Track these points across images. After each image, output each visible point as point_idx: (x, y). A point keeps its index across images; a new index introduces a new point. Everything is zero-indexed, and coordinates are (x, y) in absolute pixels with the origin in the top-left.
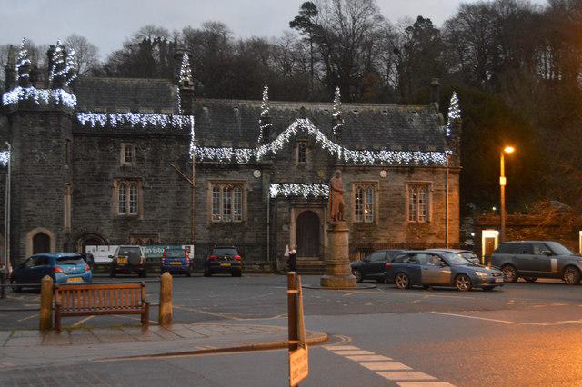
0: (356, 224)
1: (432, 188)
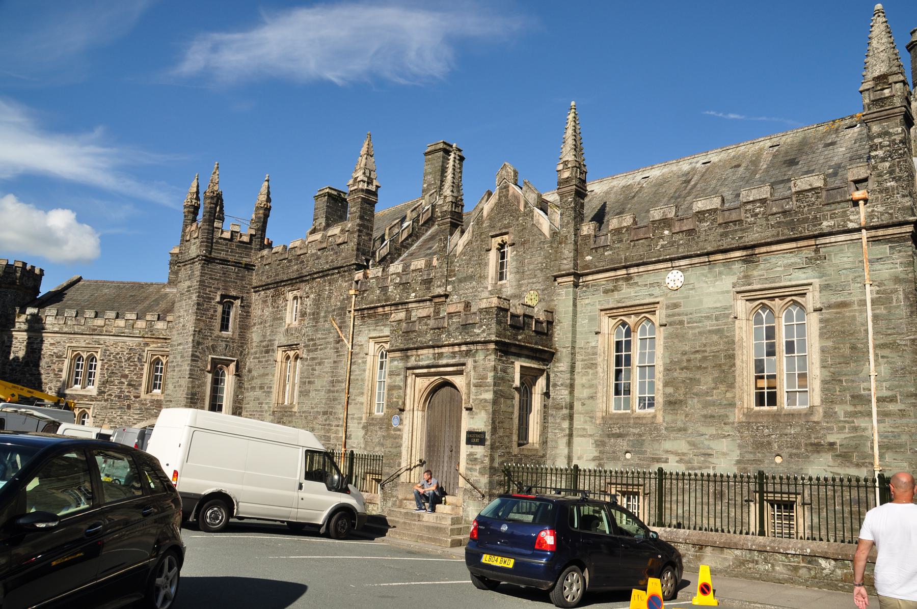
0: (609, 420)
1: (812, 299)
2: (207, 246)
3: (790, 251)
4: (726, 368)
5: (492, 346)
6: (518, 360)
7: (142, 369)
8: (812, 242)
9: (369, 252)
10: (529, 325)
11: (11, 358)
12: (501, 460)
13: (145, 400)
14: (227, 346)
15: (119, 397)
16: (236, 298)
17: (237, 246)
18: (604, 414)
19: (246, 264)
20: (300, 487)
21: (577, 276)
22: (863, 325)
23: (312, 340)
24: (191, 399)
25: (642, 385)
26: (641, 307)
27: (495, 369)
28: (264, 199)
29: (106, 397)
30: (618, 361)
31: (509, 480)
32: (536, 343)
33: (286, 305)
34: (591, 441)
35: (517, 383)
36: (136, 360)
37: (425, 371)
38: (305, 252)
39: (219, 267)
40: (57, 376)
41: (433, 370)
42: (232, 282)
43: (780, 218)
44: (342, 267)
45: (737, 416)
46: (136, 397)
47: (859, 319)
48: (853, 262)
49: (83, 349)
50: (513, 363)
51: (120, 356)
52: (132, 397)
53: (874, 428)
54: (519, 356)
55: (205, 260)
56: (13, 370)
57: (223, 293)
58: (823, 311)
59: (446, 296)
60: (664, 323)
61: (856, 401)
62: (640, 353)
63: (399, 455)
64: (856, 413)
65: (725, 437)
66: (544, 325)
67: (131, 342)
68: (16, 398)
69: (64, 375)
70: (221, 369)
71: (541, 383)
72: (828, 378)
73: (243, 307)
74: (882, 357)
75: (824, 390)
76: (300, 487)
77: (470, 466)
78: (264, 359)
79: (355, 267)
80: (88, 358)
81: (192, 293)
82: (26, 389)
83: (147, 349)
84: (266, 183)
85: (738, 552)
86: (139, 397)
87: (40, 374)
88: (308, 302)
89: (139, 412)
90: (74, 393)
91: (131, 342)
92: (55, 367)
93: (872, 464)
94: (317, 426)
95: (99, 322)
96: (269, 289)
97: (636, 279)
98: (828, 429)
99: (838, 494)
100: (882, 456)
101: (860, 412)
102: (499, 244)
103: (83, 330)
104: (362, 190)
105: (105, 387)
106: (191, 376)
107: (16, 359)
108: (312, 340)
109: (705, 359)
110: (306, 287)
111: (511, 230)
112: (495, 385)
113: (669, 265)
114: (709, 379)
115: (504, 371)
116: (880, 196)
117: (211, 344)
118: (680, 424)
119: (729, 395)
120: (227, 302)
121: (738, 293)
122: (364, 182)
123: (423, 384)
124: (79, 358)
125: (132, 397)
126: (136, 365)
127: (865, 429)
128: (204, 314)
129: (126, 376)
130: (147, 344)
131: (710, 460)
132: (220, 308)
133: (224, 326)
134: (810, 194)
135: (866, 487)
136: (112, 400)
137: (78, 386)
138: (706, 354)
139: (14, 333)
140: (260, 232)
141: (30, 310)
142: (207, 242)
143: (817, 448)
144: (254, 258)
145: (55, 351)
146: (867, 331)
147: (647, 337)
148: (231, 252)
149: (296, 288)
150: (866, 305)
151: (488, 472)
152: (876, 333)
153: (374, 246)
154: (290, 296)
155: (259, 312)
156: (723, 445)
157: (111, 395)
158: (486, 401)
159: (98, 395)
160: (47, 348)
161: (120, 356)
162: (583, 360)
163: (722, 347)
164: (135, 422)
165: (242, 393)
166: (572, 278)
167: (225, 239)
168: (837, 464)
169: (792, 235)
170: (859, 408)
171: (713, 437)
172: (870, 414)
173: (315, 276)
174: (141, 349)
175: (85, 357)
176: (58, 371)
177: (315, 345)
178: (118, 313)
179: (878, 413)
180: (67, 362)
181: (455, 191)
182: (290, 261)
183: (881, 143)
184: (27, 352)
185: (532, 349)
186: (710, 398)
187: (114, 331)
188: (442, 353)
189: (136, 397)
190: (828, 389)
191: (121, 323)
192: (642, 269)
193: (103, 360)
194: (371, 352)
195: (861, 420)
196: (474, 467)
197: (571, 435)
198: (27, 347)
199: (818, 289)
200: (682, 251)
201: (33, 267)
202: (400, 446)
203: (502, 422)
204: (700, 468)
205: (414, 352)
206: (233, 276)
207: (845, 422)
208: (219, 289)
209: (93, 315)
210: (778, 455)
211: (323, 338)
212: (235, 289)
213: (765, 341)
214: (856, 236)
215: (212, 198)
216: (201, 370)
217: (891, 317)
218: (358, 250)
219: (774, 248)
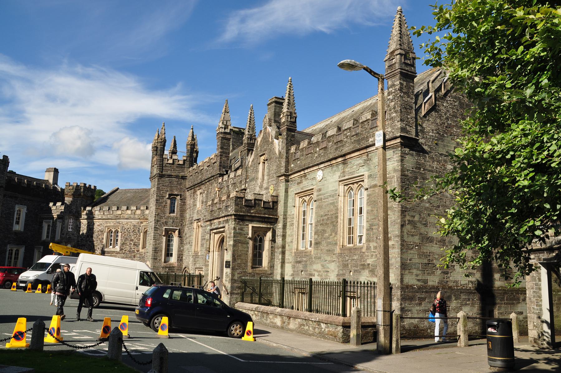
2: (160, 169)
5: (233, 217)
6: (251, 223)
7: (140, 236)
8: (365, 151)
9: (227, 166)
10: (259, 205)
11: (81, 233)
12: (239, 275)
13: (142, 252)
14: (173, 221)
15: (130, 251)
16: (177, 195)
17: (177, 167)
18: (296, 251)
19: (182, 176)
20: (137, 288)
21: (287, 176)
24: (155, 250)
26: (308, 192)
27: (234, 228)
28: (191, 139)
31: (245, 286)
32: (265, 214)
35: (250, 235)
39: (167, 179)
40: (101, 242)
42: (175, 187)
43: (355, 138)
44: (214, 176)
46: (138, 251)
49: (112, 227)
50: (248, 225)
54: (252, 221)
55: (159, 176)
56: (82, 240)
58: (369, 190)
65: (333, 262)
66: (271, 204)
67: (135, 222)
68: (69, 253)
69: (104, 241)
70: (171, 234)
71: (269, 235)
73: (182, 199)
76: (137, 288)
79: (218, 175)
80: (115, 231)
82: (74, 249)
83: (142, 225)
84: (191, 130)
85: (299, 320)
86: (139, 251)
87: (93, 241)
88: (204, 195)
90: (109, 250)
91: (135, 222)
92: (100, 237)
95: (119, 212)
96: (192, 189)
97: (308, 176)
98: (368, 256)
99: (369, 292)
103: (112, 217)
104: (221, 133)
105: (123, 247)
106: (154, 238)
107: (83, 234)
110: (203, 187)
111: (266, 152)
112: (234, 237)
115: (241, 229)
116: (389, 122)
117: (164, 221)
120: (172, 198)
122: (222, 128)
124: (111, 231)
126: (137, 234)
129: (132, 240)
130: (142, 223)
132: (169, 201)
133: (172, 211)
134: (366, 123)
135: (371, 287)
136: (126, 253)
137: (111, 247)
138: (329, 216)
139: (81, 221)
140: (189, 158)
141: (88, 208)
142: (160, 166)
143: (364, 267)
144: (189, 172)
148: (173, 170)
153: (230, 163)
155: (189, 202)
157: (126, 250)
160: (96, 228)
165: (183, 246)
167: (170, 164)
169: (358, 147)
173: (206, 181)
175: (114, 231)
178: (147, 207)
180: (105, 234)
181: (250, 131)
182: (198, 174)
184: (87, 230)
185: (261, 217)
186: (329, 240)
187: (126, 217)
188: (220, 222)
189: (138, 251)
191: (129, 212)
192: (309, 170)
198: (87, 227)
199: (367, 178)
200: (322, 160)
201: (90, 186)
203: (240, 256)
204: (325, 279)
206: (175, 183)
208: (168, 191)
209: (116, 209)
212: (176, 190)
215: (161, 142)
216: (160, 235)
218: (220, 166)
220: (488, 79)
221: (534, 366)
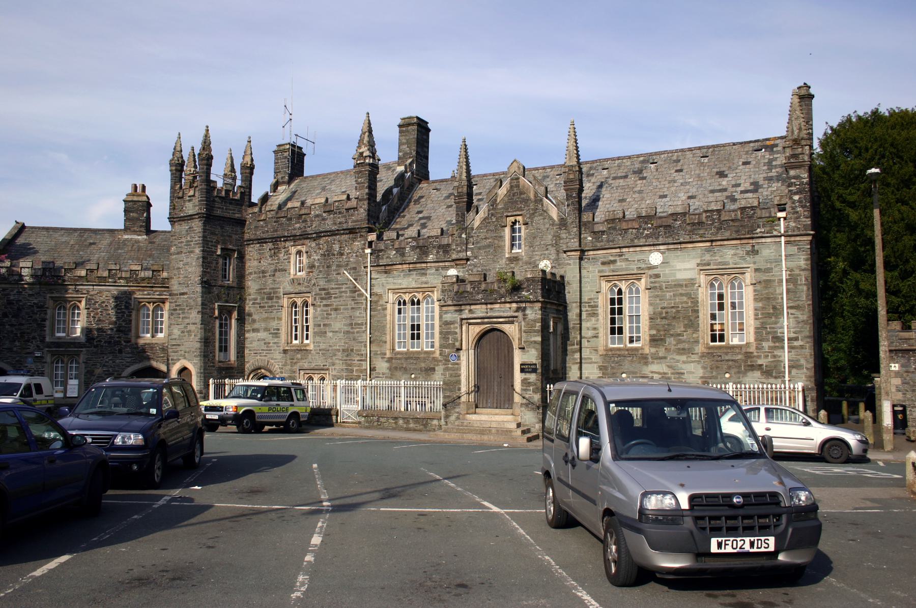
3: (736, 246)
4: (692, 318)
22: (780, 295)
23: (324, 289)
25: (631, 328)
29: (95, 343)
30: (613, 311)
33: (289, 258)
34: (596, 366)
36: (123, 307)
37: (479, 321)
38: (309, 212)
41: (486, 320)
45: (700, 349)
47: (778, 291)
48: (775, 256)
51: (106, 304)
52: (123, 342)
53: (786, 356)
57: (223, 247)
59: (468, 260)
60: (649, 287)
61: (775, 340)
62: (629, 307)
63: (459, 382)
64: (775, 347)
72: (759, 326)
74: (791, 314)
75: (756, 333)
77: (525, 388)
78: (266, 305)
81: (194, 248)
86: (130, 341)
89: (131, 356)
93: (784, 377)
94: (337, 361)
100: (790, 372)
101: (778, 347)
102: (512, 222)
108: (324, 289)
109: (678, 312)
113: (652, 248)
114: (682, 325)
118: (661, 354)
119: (694, 335)
121: (701, 270)
123: (476, 330)
125: (123, 342)
126: (124, 313)
127: (780, 356)
128: (209, 267)
131: (682, 376)
136: (102, 346)
145: (35, 301)
146: (782, 298)
147: (634, 295)
148: (226, 209)
149: (300, 244)
150: (782, 282)
151: (540, 391)
152: (787, 300)
154: (293, 250)
156: (691, 367)
157: (100, 341)
158: (535, 342)
159: (86, 342)
161: (106, 304)
162: (587, 311)
163: (690, 304)
164: (128, 364)
165: (244, 335)
166: (578, 253)
168: (763, 377)
170: (777, 344)
171: (684, 362)
172: (783, 348)
174: (127, 297)
176: (41, 321)
177: (328, 293)
179: (789, 347)
183: (795, 182)
190: (758, 332)
192: (631, 249)
193: (88, 309)
194: (391, 301)
195: (779, 351)
196: (528, 388)
197: (581, 363)
202: (460, 376)
205: (468, 307)
207: (769, 352)
210: (727, 373)
211: (337, 288)
213: (717, 302)
214: (777, 240)
217: (797, 291)
219: (726, 243)
220: (422, 160)
221: (669, 451)
